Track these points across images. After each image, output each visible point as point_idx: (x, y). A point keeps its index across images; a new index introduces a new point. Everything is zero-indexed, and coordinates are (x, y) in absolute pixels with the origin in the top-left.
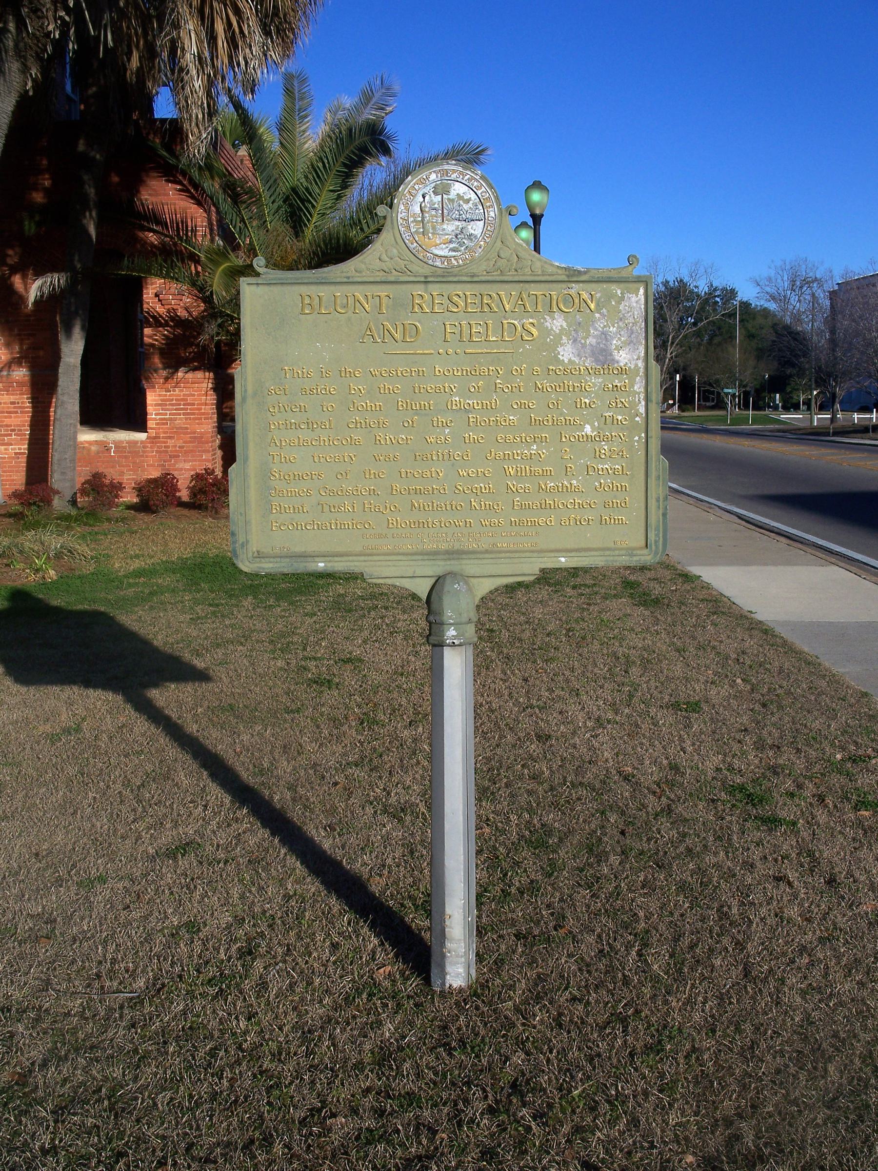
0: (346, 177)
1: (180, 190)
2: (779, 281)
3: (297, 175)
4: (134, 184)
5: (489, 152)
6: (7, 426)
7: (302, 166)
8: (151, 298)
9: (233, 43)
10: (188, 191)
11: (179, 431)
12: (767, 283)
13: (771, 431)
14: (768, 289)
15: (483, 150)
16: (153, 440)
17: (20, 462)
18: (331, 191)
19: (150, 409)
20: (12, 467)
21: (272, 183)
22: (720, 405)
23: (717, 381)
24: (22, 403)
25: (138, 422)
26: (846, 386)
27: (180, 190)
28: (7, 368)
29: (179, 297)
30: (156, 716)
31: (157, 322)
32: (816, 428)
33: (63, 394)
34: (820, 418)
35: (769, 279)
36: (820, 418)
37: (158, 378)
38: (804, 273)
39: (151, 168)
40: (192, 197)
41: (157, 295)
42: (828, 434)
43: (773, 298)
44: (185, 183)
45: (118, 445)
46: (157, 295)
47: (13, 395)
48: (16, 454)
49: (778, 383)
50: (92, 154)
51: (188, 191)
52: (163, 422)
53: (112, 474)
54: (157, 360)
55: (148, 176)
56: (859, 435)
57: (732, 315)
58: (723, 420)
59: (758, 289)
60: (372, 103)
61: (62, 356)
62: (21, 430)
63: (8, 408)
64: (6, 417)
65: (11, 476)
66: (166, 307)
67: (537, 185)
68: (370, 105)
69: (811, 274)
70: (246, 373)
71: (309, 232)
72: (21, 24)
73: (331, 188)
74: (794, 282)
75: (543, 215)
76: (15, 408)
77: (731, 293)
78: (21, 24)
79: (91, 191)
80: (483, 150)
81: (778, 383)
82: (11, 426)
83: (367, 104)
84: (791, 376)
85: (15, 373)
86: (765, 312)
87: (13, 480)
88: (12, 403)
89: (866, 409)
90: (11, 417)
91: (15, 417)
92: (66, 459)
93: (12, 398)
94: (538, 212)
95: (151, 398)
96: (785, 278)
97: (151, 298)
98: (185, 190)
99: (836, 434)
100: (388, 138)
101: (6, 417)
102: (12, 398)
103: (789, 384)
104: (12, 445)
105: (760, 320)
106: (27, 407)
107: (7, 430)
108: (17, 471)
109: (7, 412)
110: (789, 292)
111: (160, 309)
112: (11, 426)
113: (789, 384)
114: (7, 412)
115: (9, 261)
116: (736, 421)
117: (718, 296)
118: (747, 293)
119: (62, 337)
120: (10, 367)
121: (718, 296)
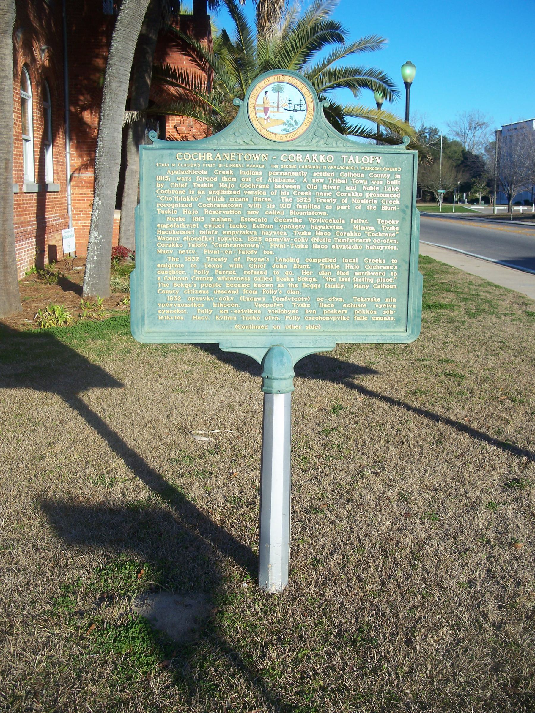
1: (191, 60)
2: (462, 124)
4: (162, 54)
5: (386, 42)
6: (77, 208)
8: (171, 129)
10: (196, 61)
12: (454, 125)
13: (471, 216)
14: (455, 129)
15: (383, 41)
17: (86, 232)
18: (296, 64)
20: (80, 234)
22: (434, 200)
23: (432, 186)
24: (88, 194)
26: (517, 190)
27: (191, 60)
28: (78, 171)
29: (189, 129)
30: (362, 390)
32: (496, 215)
33: (129, 189)
34: (499, 209)
35: (456, 123)
36: (499, 209)
38: (477, 119)
39: (174, 46)
40: (199, 65)
41: (175, 127)
42: (509, 219)
43: (458, 134)
44: (194, 56)
46: (175, 127)
47: (82, 189)
48: (83, 226)
49: (465, 188)
50: (151, 35)
51: (196, 61)
55: (172, 51)
56: (529, 220)
57: (437, 144)
58: (437, 209)
59: (449, 129)
60: (321, 8)
61: (128, 164)
62: (86, 211)
63: (78, 197)
64: (77, 203)
65: (79, 240)
66: (181, 135)
67: (409, 63)
68: (320, 10)
69: (481, 120)
73: (296, 62)
74: (470, 124)
75: (412, 83)
76: (82, 197)
77: (434, 131)
80: (383, 41)
81: (465, 188)
82: (80, 208)
83: (317, 10)
84: (474, 182)
85: (83, 175)
86: (455, 143)
87: (81, 243)
88: (81, 194)
89: (528, 203)
90: (80, 203)
91: (83, 203)
92: (129, 230)
93: (81, 191)
94: (409, 81)
96: (465, 122)
97: (171, 129)
98: (194, 61)
99: (514, 219)
100: (342, 32)
101: (77, 203)
102: (81, 191)
103: (473, 188)
104: (80, 220)
105: (454, 148)
106: (91, 197)
107: (78, 211)
108: (83, 237)
109: (78, 200)
110: (467, 131)
112: (80, 208)
113: (473, 188)
114: (78, 200)
115: (81, 103)
116: (445, 210)
117: (427, 133)
118: (444, 131)
119: (45, 151)
120: (80, 170)
121: (427, 133)
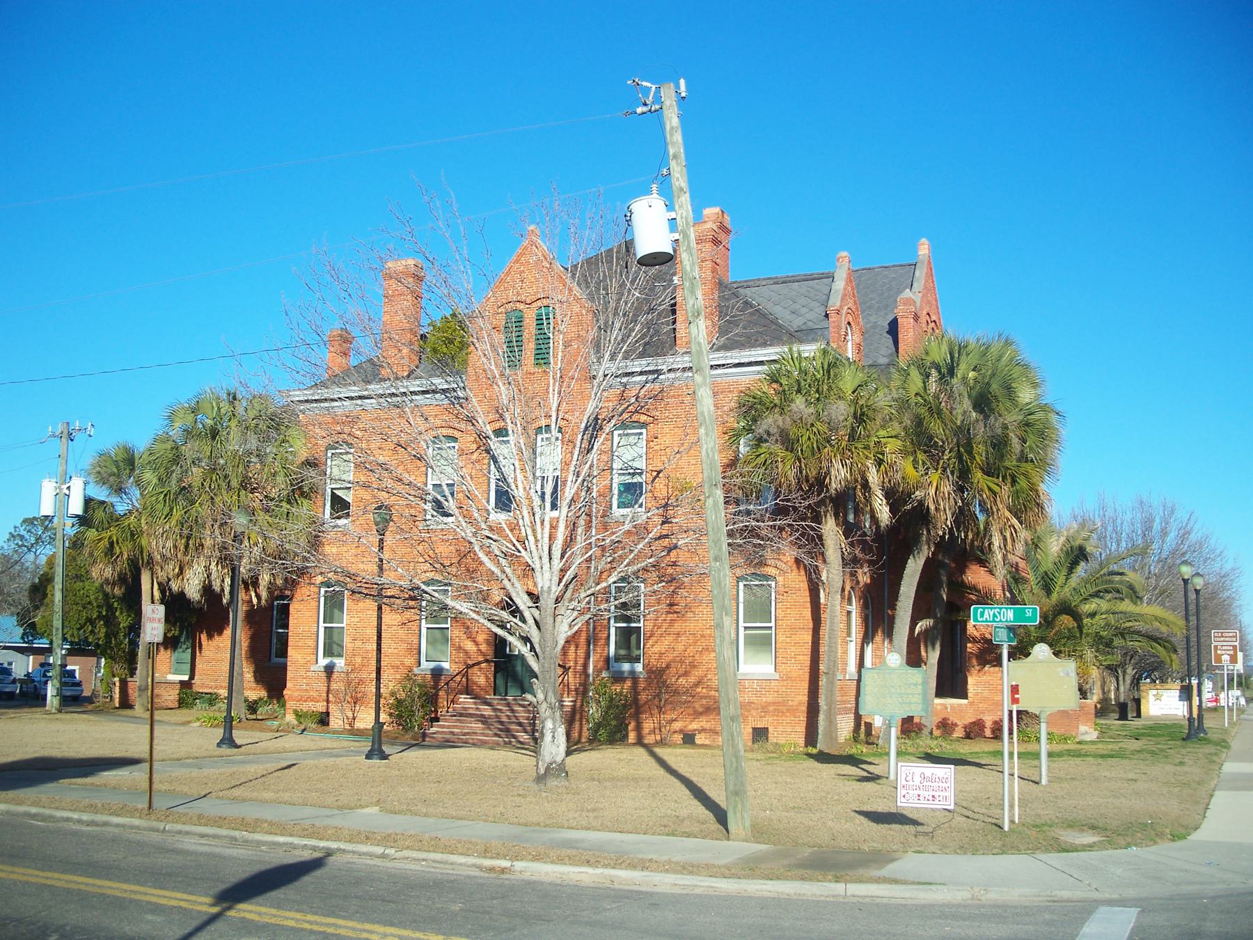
0: (1071, 570)
3: (1047, 565)
4: (962, 569)
7: (1051, 559)
9: (1013, 540)
11: (984, 700)
16: (971, 703)
19: (969, 687)
21: (1036, 569)
25: (966, 697)
31: (974, 640)
37: (974, 671)
45: (952, 707)
52: (977, 694)
53: (953, 719)
54: (974, 661)
70: (178, 711)
71: (1055, 596)
72: (929, 531)
78: (929, 531)
79: (944, 578)
95: (970, 680)
111: (976, 634)
